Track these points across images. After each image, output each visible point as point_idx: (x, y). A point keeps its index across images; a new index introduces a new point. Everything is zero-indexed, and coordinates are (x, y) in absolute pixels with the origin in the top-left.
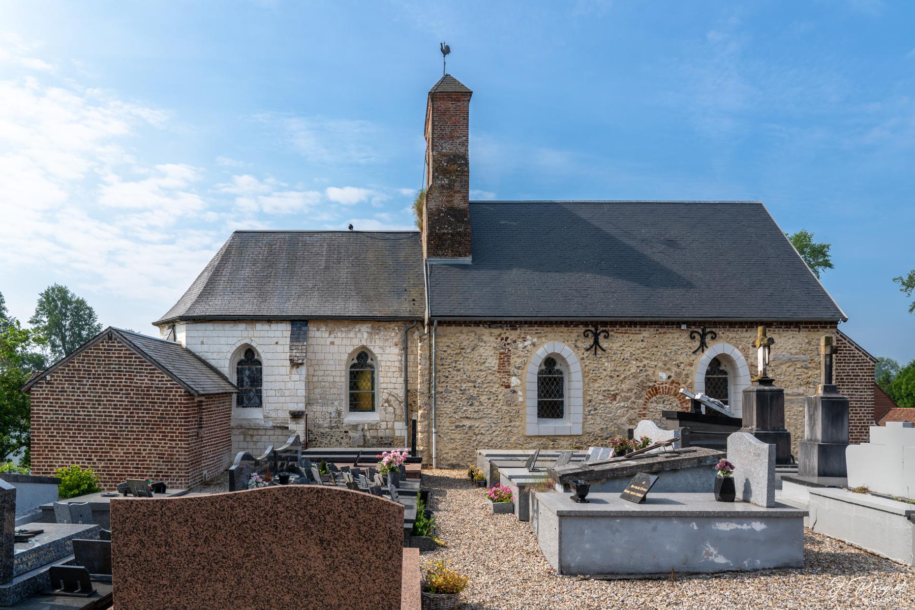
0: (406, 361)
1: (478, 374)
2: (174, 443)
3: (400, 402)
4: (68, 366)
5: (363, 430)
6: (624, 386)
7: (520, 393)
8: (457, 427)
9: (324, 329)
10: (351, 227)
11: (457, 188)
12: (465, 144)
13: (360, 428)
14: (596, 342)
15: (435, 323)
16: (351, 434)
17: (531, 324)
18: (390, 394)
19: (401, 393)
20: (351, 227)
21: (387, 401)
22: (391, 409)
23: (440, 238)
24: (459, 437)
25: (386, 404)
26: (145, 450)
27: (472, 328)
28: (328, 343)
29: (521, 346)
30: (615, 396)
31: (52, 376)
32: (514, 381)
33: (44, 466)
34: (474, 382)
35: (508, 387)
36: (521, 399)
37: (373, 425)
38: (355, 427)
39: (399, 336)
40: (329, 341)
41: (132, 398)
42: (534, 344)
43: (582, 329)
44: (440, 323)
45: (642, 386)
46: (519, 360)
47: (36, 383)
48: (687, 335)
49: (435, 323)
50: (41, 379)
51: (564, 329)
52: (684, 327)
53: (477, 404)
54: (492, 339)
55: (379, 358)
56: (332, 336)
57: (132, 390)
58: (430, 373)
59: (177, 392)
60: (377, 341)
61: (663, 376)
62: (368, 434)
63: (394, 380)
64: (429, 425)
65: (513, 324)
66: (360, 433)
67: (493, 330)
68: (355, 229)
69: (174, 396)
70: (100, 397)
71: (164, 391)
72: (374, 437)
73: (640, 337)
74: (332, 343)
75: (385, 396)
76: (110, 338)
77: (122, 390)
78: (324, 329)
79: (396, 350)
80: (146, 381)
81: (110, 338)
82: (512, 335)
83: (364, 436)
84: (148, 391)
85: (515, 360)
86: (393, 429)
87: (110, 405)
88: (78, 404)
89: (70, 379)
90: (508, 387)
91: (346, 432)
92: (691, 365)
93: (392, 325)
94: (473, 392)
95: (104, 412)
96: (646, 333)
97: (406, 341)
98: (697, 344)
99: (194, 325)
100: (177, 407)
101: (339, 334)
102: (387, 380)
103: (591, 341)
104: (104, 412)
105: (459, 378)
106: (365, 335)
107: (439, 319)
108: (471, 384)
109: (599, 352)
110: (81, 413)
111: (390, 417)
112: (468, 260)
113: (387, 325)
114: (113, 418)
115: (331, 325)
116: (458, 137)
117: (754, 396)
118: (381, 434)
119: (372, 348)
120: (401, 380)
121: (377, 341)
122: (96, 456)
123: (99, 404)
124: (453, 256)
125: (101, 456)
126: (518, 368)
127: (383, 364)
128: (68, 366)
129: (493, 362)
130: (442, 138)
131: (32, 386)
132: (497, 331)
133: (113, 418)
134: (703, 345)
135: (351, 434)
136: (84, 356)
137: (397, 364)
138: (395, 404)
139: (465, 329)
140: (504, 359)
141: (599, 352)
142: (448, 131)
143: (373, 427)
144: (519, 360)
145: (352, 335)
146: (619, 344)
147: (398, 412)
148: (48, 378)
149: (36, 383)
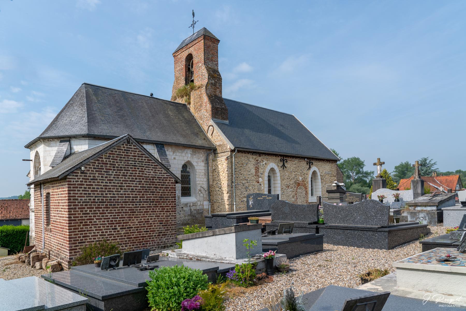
0: (208, 169)
1: (248, 176)
2: (168, 213)
3: (206, 191)
4: (98, 160)
5: (190, 206)
6: (291, 183)
7: (262, 185)
8: (242, 201)
9: (170, 150)
10: (152, 95)
11: (218, 86)
12: (217, 65)
13: (188, 205)
14: (284, 165)
15: (236, 151)
16: (184, 209)
17: (265, 154)
18: (201, 187)
19: (205, 186)
20: (152, 95)
21: (200, 190)
22: (202, 195)
23: (217, 110)
24: (242, 206)
25: (200, 192)
26: (151, 219)
27: (247, 155)
28: (173, 158)
29: (262, 164)
30: (289, 186)
31: (86, 168)
32: (260, 180)
33: (79, 237)
34: (247, 180)
35: (258, 182)
36: (263, 188)
37: (194, 203)
38: (186, 205)
39: (204, 157)
40: (173, 157)
41: (143, 184)
42: (266, 164)
43: (280, 158)
44: (239, 151)
45: (295, 182)
46: (262, 170)
47: (72, 172)
48: (306, 163)
49: (236, 151)
50: (77, 169)
51: (274, 157)
52: (306, 159)
53: (248, 190)
54: (253, 160)
55: (196, 168)
56: (175, 154)
57: (143, 179)
58: (232, 176)
59: (170, 180)
60: (195, 159)
61: (301, 178)
62: (192, 208)
63: (202, 180)
64: (232, 201)
65: (260, 154)
66: (189, 208)
67: (253, 156)
68: (154, 96)
69: (168, 183)
70: (122, 183)
71: (163, 180)
72: (195, 210)
73: (294, 163)
74: (175, 158)
75: (199, 188)
76: (128, 142)
77: (136, 179)
78: (170, 150)
79: (203, 164)
80: (152, 173)
81: (128, 142)
82: (260, 159)
83: (191, 209)
84: (153, 180)
85: (261, 171)
86: (203, 205)
87: (129, 189)
88: (106, 189)
89: (99, 170)
90: (258, 182)
91: (182, 208)
92: (307, 174)
93: (201, 151)
94: (247, 185)
95: (125, 194)
96: (296, 161)
97: (207, 160)
98: (308, 166)
99: (95, 141)
100: (170, 190)
101: (178, 154)
102: (199, 179)
103: (282, 164)
104: (125, 194)
105: (242, 178)
106: (190, 155)
107: (238, 149)
108: (246, 181)
109: (285, 168)
110: (108, 195)
111: (201, 199)
112: (227, 122)
113: (199, 150)
114: (131, 199)
115: (174, 148)
116: (215, 61)
117: (381, 181)
118: (198, 208)
119: (193, 162)
120: (205, 180)
121: (195, 159)
122: (119, 226)
123: (121, 189)
124: (222, 119)
125: (123, 226)
126: (262, 174)
127: (198, 171)
128: (98, 160)
129: (253, 171)
130: (208, 59)
131: (68, 175)
132: (254, 157)
133: (131, 199)
134: (310, 167)
135: (184, 209)
136: (110, 154)
137: (203, 171)
138: (203, 192)
139: (244, 155)
140: (257, 169)
141: (285, 168)
142: (210, 56)
143: (194, 204)
144: (262, 170)
145: (183, 154)
146: (291, 164)
147: (205, 196)
148: (83, 168)
149: (72, 172)
